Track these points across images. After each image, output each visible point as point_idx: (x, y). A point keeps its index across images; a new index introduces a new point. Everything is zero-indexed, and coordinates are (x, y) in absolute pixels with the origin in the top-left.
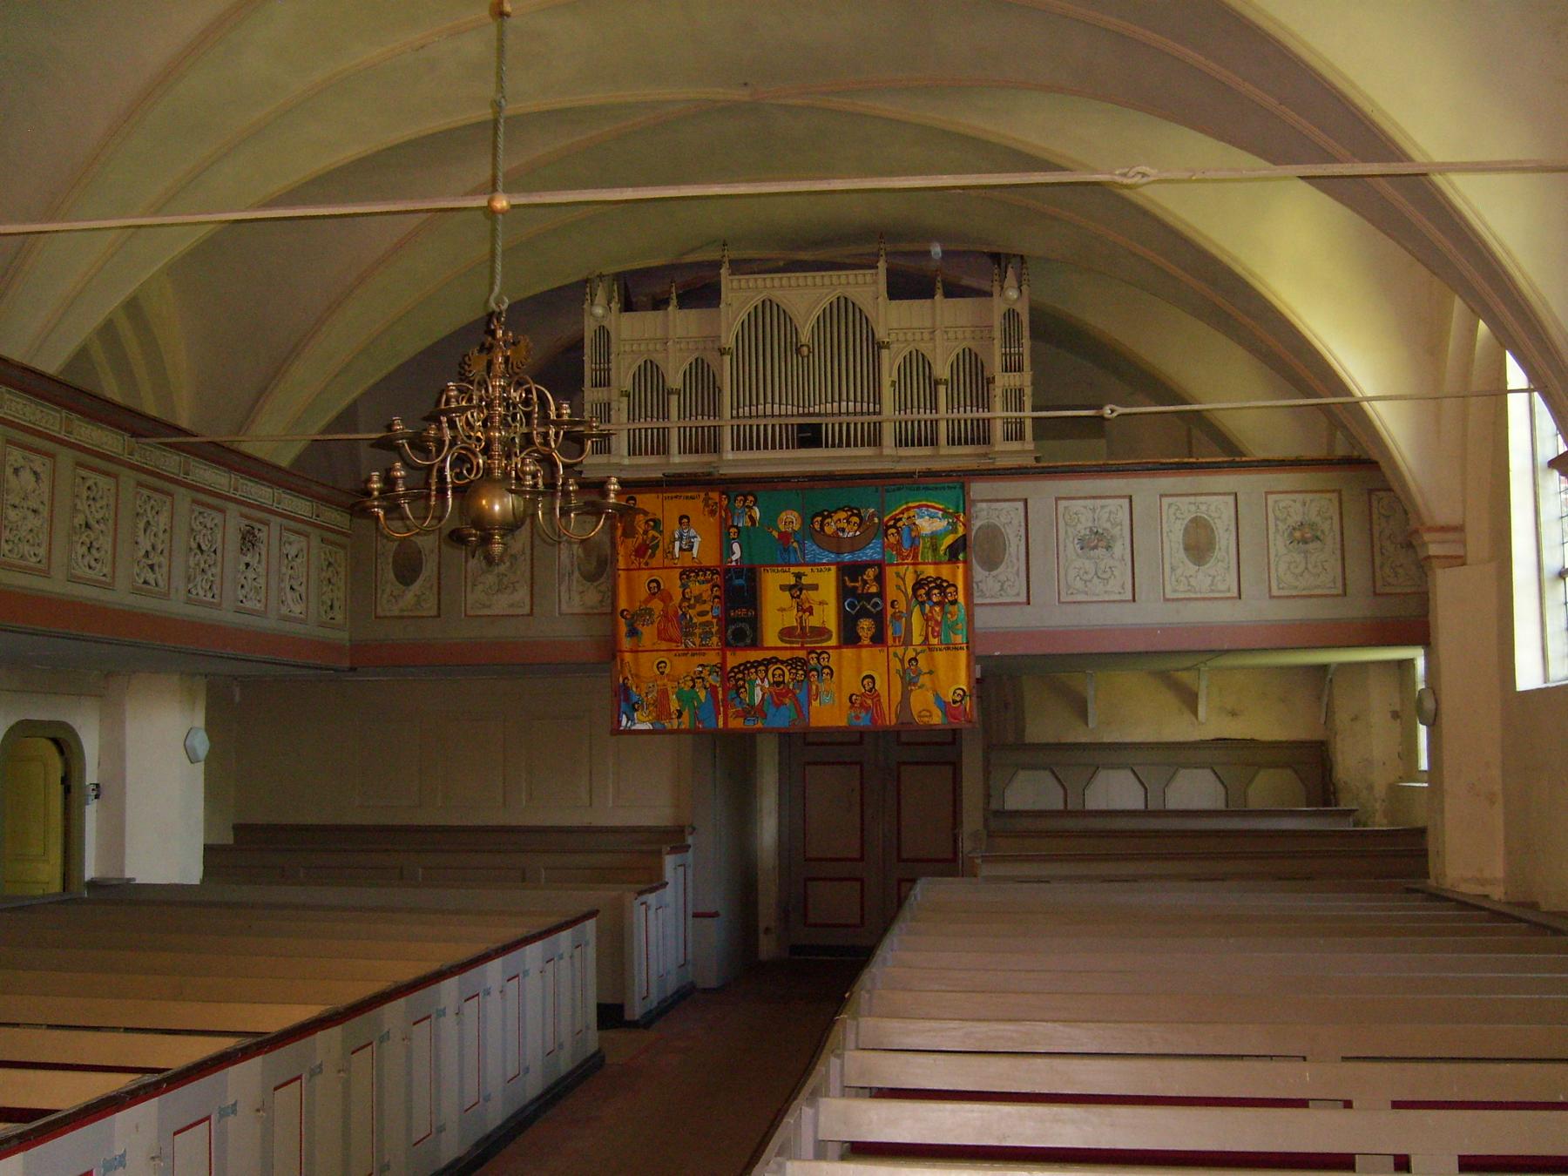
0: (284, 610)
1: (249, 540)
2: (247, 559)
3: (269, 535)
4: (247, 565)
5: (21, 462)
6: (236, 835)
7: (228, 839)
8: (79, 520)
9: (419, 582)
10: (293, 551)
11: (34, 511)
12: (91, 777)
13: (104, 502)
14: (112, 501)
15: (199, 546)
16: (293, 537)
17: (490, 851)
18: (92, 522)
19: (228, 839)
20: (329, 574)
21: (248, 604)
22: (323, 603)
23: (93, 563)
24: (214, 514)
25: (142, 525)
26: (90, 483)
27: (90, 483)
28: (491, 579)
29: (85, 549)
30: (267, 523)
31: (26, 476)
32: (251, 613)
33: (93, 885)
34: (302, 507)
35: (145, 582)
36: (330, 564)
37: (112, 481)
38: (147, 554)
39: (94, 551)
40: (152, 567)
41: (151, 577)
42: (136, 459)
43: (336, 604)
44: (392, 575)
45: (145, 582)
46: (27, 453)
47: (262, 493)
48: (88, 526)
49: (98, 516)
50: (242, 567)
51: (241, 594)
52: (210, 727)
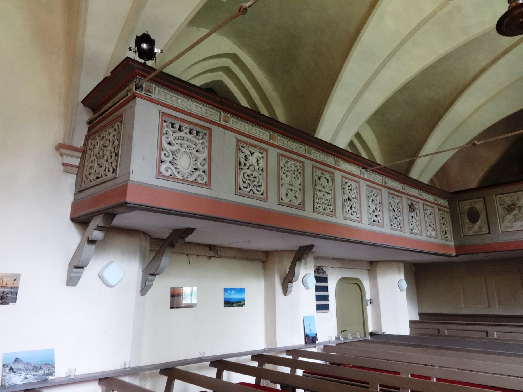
0: (428, 233)
1: (412, 208)
2: (412, 214)
3: (419, 206)
4: (412, 217)
5: (320, 175)
6: (411, 328)
7: (417, 318)
8: (346, 197)
9: (478, 223)
10: (429, 212)
11: (328, 193)
12: (368, 296)
13: (355, 191)
14: (358, 191)
15: (393, 209)
16: (428, 208)
17: (202, 256)
18: (352, 199)
19: (417, 318)
20: (443, 222)
21: (415, 231)
22: (443, 232)
23: (353, 213)
24: (397, 198)
25: (370, 200)
26: (348, 184)
27: (348, 184)
28: (510, 217)
29: (349, 208)
30: (418, 203)
31: (323, 180)
32: (415, 234)
33: (371, 334)
34: (430, 198)
35: (374, 221)
36: (443, 218)
37: (357, 184)
38: (374, 211)
39: (353, 209)
40: (376, 216)
41: (376, 219)
42: (365, 177)
43: (448, 232)
44: (467, 220)
45: (374, 221)
46: (322, 172)
47: (415, 192)
48: (349, 200)
49: (354, 196)
50: (410, 217)
51: (411, 227)
52: (406, 279)
